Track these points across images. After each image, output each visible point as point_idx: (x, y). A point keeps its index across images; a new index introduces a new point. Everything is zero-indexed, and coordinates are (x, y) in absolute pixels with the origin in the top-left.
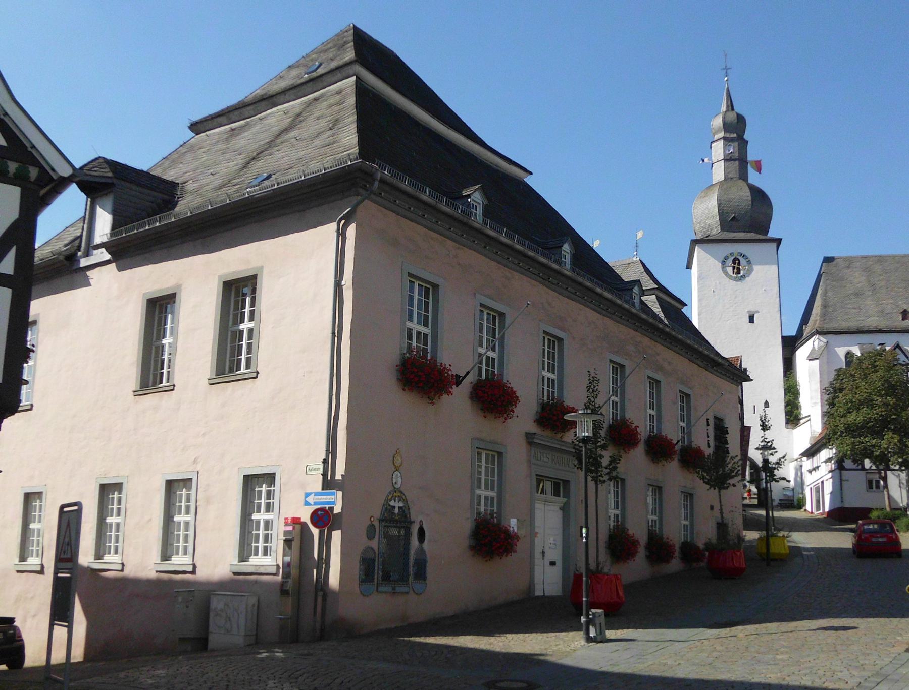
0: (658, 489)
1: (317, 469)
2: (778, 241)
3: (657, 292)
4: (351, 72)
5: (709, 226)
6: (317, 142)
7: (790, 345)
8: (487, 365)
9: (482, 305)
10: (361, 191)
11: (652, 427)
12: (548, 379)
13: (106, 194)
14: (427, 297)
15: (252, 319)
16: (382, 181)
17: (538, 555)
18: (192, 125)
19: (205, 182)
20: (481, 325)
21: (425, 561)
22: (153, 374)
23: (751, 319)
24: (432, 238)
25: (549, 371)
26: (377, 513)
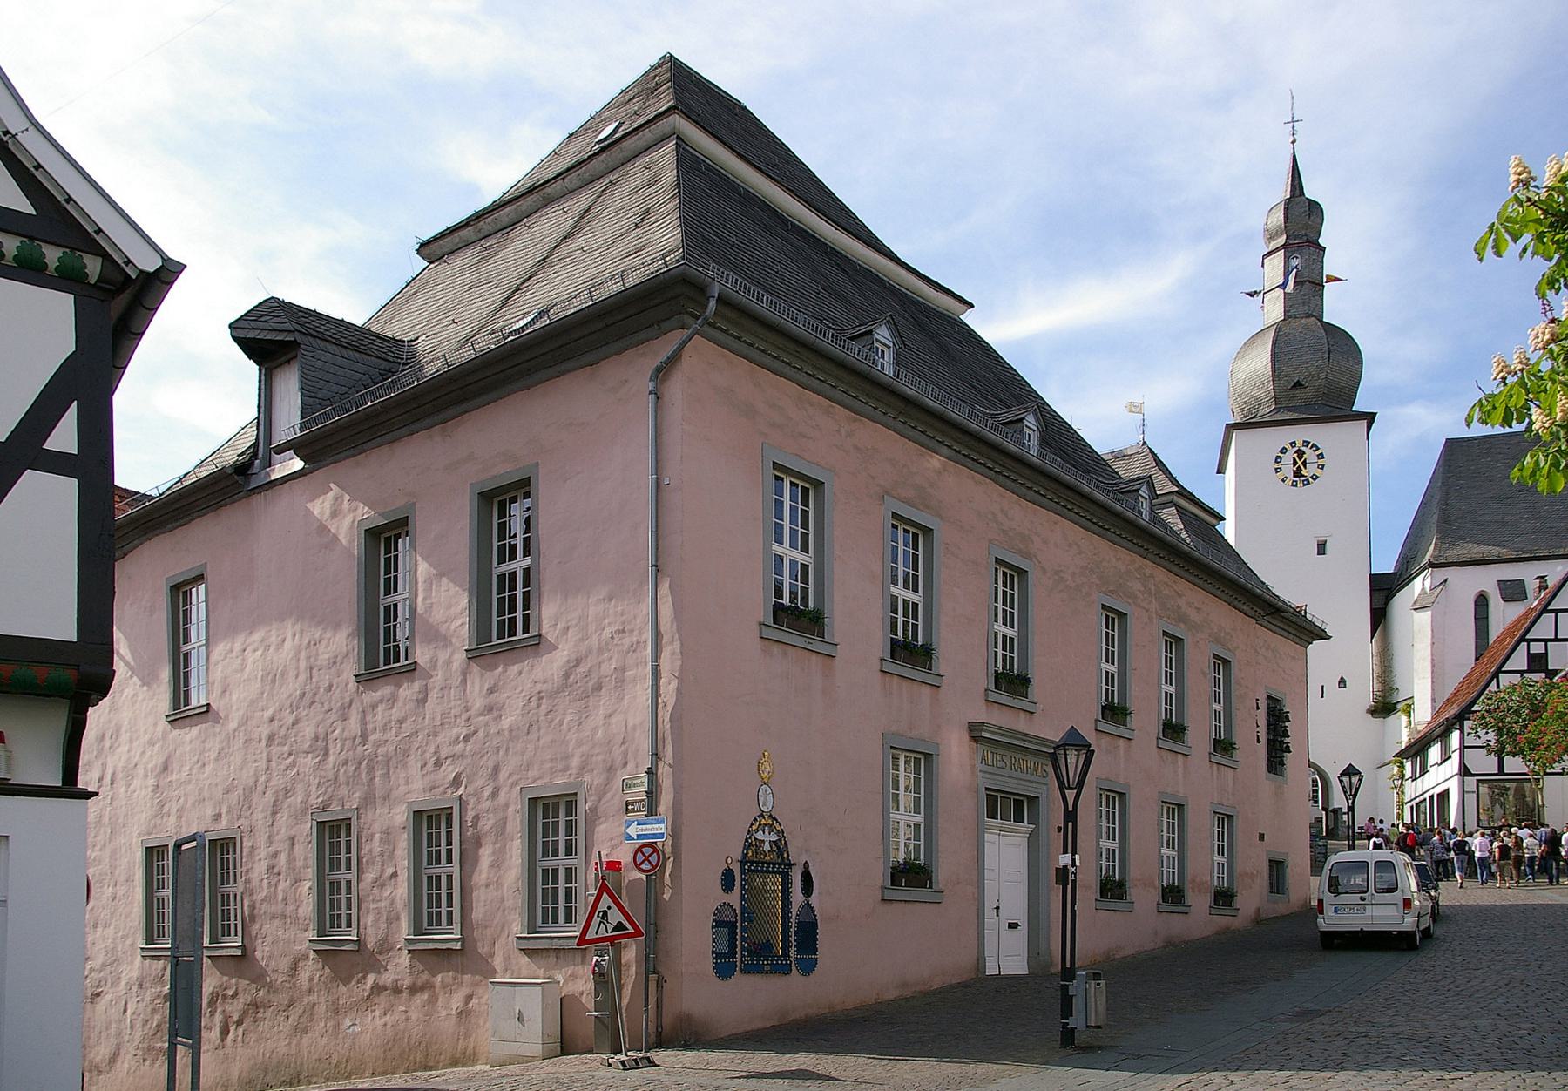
1: (639, 785)
2: (1370, 418)
3: (1176, 499)
4: (667, 130)
5: (1256, 399)
6: (616, 251)
7: (1384, 589)
8: (906, 615)
9: (895, 515)
10: (687, 319)
11: (1168, 712)
12: (1004, 637)
13: (288, 362)
14: (805, 502)
15: (526, 553)
16: (722, 300)
17: (989, 912)
18: (422, 245)
19: (443, 336)
20: (895, 549)
21: (815, 925)
22: (384, 655)
23: (1322, 548)
24: (812, 405)
26: (737, 854)
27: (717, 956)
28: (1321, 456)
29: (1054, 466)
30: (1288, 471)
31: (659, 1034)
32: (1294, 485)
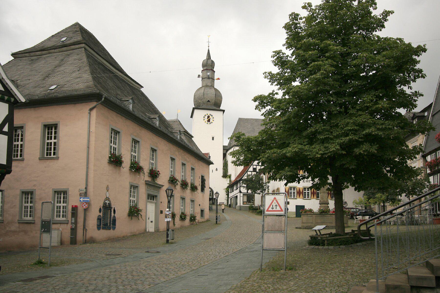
0: (183, 199)
17: (147, 219)
25: (114, 144)
26: (102, 205)
27: (98, 225)
28: (213, 118)
29: (163, 129)
30: (206, 120)
31: (85, 241)
32: (207, 123)
